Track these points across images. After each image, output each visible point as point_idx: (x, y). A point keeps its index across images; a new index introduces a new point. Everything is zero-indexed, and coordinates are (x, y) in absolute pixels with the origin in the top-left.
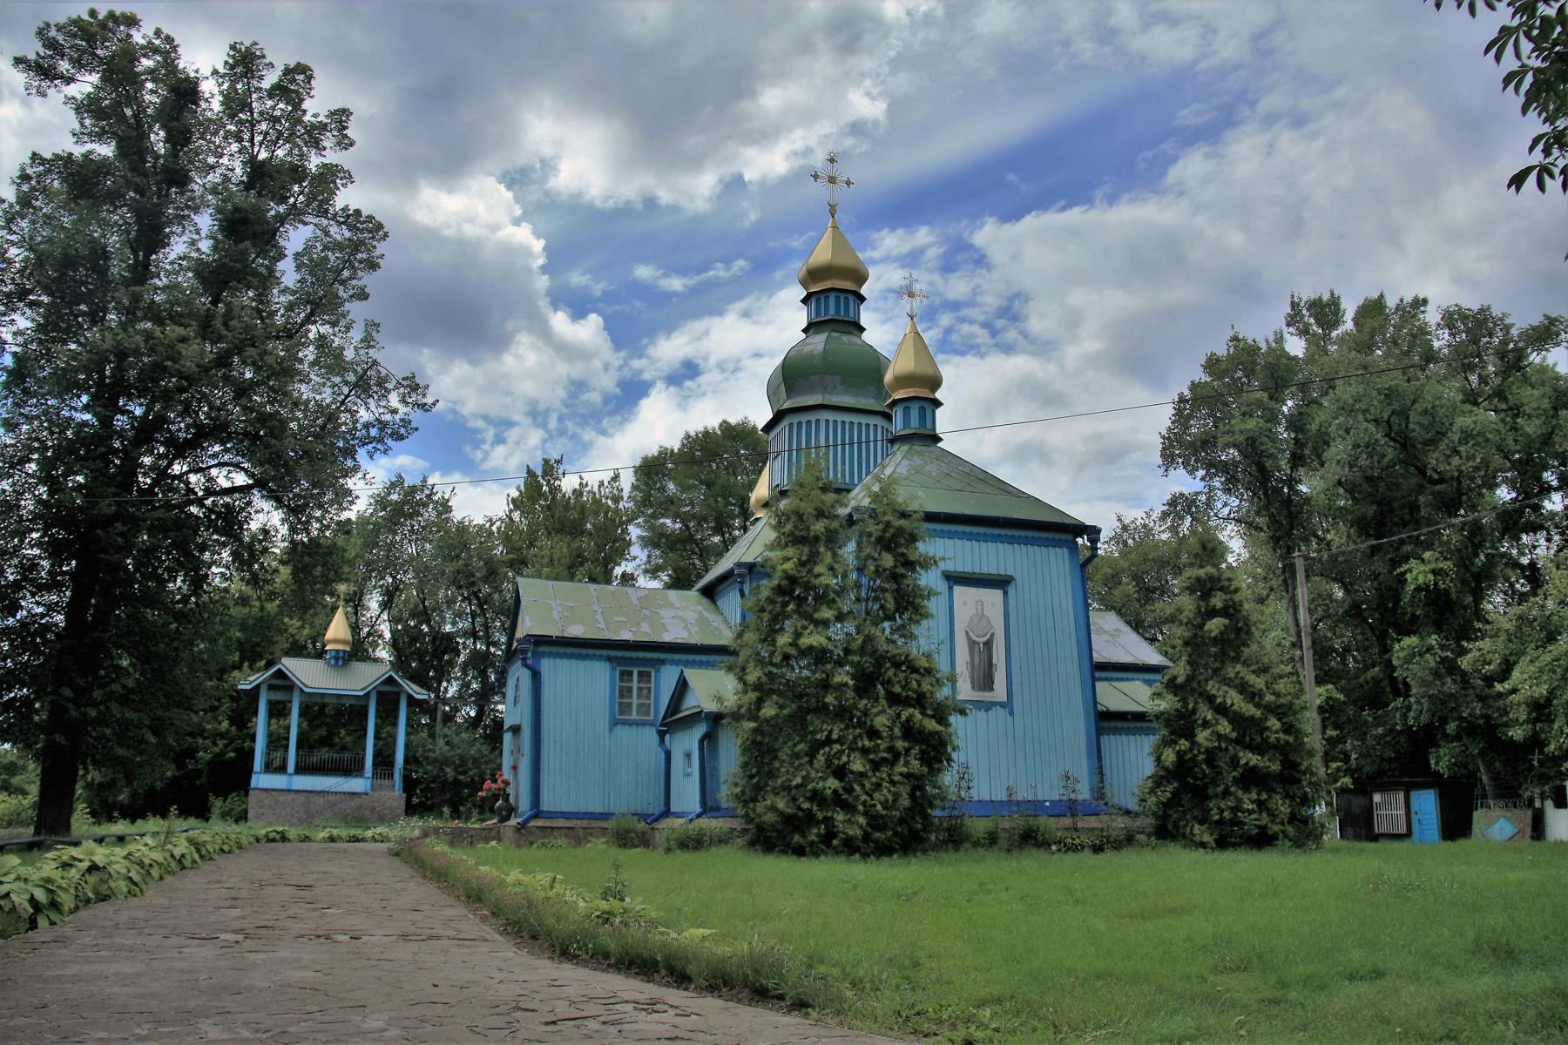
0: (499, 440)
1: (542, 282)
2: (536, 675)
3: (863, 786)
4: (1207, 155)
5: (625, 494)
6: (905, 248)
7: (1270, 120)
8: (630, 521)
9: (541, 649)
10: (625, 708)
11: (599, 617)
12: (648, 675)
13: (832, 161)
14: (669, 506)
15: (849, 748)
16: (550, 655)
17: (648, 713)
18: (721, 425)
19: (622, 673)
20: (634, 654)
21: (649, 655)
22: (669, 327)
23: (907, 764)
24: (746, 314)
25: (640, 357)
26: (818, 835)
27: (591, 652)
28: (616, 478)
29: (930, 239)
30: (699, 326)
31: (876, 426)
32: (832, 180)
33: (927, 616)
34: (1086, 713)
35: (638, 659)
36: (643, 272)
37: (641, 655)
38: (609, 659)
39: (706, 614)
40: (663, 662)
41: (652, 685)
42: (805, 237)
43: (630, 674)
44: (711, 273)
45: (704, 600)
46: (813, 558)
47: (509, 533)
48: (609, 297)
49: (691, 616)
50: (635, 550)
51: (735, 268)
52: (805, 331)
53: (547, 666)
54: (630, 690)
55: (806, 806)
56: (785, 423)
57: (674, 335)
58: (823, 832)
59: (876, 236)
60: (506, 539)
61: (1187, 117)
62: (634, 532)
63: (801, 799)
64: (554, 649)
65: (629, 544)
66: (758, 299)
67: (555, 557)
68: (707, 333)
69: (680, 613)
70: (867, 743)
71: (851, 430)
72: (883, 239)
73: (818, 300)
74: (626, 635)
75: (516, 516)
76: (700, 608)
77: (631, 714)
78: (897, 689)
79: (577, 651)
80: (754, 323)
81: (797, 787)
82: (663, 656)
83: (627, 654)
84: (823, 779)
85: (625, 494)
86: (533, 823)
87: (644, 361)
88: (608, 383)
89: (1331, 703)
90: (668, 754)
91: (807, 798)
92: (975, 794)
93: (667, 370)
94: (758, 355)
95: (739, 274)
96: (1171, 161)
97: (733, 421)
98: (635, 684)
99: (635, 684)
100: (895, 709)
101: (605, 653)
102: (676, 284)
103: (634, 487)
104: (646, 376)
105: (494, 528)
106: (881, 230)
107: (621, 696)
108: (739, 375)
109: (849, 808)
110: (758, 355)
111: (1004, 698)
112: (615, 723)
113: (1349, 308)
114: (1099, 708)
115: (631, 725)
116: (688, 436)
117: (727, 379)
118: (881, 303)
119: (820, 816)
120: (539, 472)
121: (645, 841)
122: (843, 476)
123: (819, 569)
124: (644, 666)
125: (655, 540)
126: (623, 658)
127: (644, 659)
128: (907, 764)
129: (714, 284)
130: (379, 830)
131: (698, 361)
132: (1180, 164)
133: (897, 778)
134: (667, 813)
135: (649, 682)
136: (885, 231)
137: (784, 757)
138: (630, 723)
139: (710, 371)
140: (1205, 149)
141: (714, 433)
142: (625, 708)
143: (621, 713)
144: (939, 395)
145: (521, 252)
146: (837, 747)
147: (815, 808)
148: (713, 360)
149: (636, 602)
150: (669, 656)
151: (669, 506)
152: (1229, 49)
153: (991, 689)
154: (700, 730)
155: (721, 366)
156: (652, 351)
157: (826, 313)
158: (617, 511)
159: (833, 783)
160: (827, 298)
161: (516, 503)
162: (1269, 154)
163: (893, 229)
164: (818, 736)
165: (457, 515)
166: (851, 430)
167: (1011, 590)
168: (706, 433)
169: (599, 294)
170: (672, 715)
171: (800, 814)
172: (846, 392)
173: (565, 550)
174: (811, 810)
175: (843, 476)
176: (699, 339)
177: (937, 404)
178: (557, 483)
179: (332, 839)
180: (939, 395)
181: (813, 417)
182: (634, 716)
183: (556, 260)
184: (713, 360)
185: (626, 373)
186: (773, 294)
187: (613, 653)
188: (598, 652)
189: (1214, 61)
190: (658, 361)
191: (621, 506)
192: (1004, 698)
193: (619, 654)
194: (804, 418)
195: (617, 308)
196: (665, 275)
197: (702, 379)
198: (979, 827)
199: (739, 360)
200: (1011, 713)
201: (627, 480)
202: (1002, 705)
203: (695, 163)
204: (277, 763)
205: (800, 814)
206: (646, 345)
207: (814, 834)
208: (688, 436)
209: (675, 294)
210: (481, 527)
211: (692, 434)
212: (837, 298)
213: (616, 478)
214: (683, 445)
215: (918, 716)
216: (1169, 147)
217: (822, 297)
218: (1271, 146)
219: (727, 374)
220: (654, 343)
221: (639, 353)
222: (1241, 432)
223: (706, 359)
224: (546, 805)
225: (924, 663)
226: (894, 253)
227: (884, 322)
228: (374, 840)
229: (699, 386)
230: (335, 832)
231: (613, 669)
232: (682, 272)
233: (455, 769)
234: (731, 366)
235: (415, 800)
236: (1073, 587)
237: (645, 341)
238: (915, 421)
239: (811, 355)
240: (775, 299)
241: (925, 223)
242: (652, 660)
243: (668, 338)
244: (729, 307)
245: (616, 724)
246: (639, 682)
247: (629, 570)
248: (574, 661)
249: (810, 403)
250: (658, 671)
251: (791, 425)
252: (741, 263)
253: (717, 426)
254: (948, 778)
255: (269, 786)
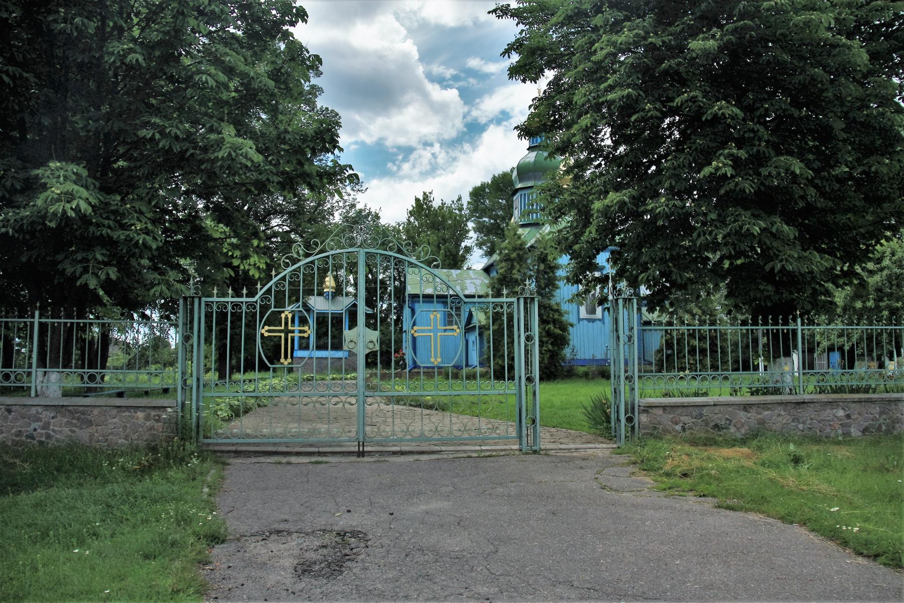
0: (405, 159)
1: (420, 70)
5: (465, 207)
9: (415, 299)
14: (484, 212)
23: (547, 347)
28: (460, 199)
33: (558, 288)
45: (485, 274)
46: (512, 267)
47: (409, 228)
48: (455, 78)
49: (478, 282)
50: (472, 234)
57: (493, 97)
62: (471, 225)
65: (468, 231)
67: (431, 241)
69: (474, 281)
75: (412, 219)
76: (482, 278)
78: (545, 317)
86: (414, 371)
90: (467, 342)
92: (578, 357)
100: (544, 325)
105: (401, 228)
107: (449, 318)
111: (600, 317)
120: (421, 198)
121: (456, 376)
123: (514, 271)
125: (479, 229)
128: (547, 347)
130: (353, 375)
131: (508, 110)
133: (543, 352)
139: (516, 116)
145: (406, 55)
153: (595, 314)
158: (461, 216)
161: (411, 213)
165: (383, 221)
173: (435, 238)
179: (333, 379)
183: (427, 55)
185: (469, 119)
190: (486, 111)
191: (463, 213)
192: (600, 317)
194: (527, 192)
196: (486, 64)
198: (581, 369)
200: (604, 323)
201: (466, 199)
202: (599, 320)
204: (304, 345)
206: (478, 103)
208: (494, 177)
210: (395, 228)
211: (497, 175)
213: (460, 199)
215: (552, 328)
220: (482, 102)
223: (513, 109)
225: (555, 307)
228: (351, 379)
230: (334, 376)
233: (386, 346)
235: (369, 360)
239: (529, 163)
247: (469, 245)
249: (529, 185)
251: (521, 195)
254: (567, 352)
255: (302, 356)
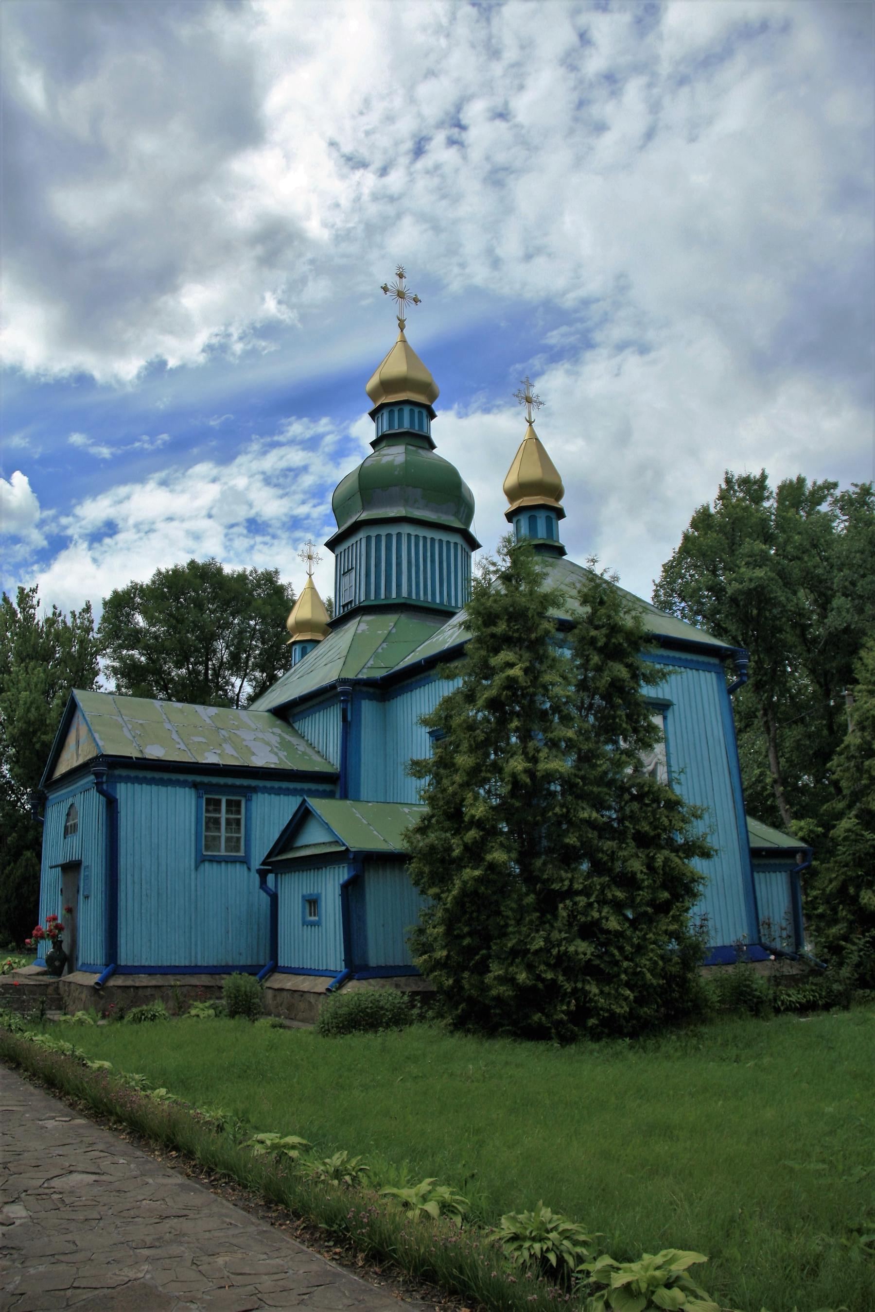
2: (112, 805)
3: (621, 949)
4: (568, 373)
5: (96, 626)
6: (308, 434)
7: (621, 347)
8: (97, 653)
9: (117, 772)
10: (212, 843)
11: (175, 736)
12: (238, 804)
13: (401, 276)
15: (598, 902)
16: (128, 780)
17: (237, 849)
18: (189, 564)
19: (208, 801)
20: (222, 781)
21: (238, 782)
22: (95, 491)
24: (164, 483)
25: (67, 515)
26: (568, 1013)
27: (174, 777)
29: (329, 428)
30: (123, 490)
31: (456, 544)
32: (401, 295)
34: (741, 848)
35: (226, 786)
36: (77, 439)
37: (230, 781)
38: (195, 786)
39: (288, 737)
40: (255, 790)
41: (242, 816)
42: (223, 418)
43: (218, 802)
44: (137, 444)
51: (159, 442)
52: (374, 444)
53: (123, 791)
54: (217, 821)
55: (549, 976)
56: (362, 535)
57: (99, 498)
58: (573, 1007)
59: (284, 421)
60: (720, 526)
61: (554, 338)
63: (542, 967)
64: (133, 773)
65: (96, 674)
66: (176, 471)
68: (128, 497)
70: (620, 894)
71: (433, 546)
72: (290, 424)
73: (391, 413)
74: (211, 758)
76: (278, 731)
77: (219, 851)
78: (645, 827)
79: (157, 775)
80: (172, 491)
81: (537, 952)
82: (253, 783)
83: (215, 780)
84: (570, 941)
85: (96, 626)
87: (70, 519)
88: (38, 539)
89: (812, 835)
90: (274, 899)
91: (548, 965)
93: (90, 529)
94: (170, 519)
95: (161, 447)
96: (539, 374)
97: (200, 561)
98: (223, 816)
99: (223, 816)
101: (191, 778)
102: (105, 452)
103: (105, 619)
104: (69, 532)
106: (289, 417)
108: (152, 536)
109: (603, 977)
110: (170, 519)
112: (201, 860)
113: (773, 484)
114: (752, 845)
115: (219, 862)
116: (159, 573)
117: (141, 539)
118: (281, 480)
119: (568, 987)
122: (418, 594)
124: (234, 794)
126: (211, 785)
127: (233, 786)
129: (140, 454)
132: (545, 377)
134: (275, 968)
135: (238, 812)
136: (293, 418)
137: (510, 913)
138: (217, 860)
139: (128, 531)
140: (567, 366)
141: (183, 572)
142: (212, 843)
143: (207, 848)
144: (562, 503)
146: (582, 900)
147: (561, 978)
148: (131, 522)
149: (208, 721)
150: (260, 783)
151: (135, 638)
152: (594, 285)
154: (341, 874)
155: (137, 526)
156: (78, 511)
157: (401, 424)
159: (583, 948)
160: (401, 411)
162: (617, 375)
163: (300, 417)
164: (556, 886)
166: (433, 546)
167: (670, 715)
168: (176, 571)
169: (37, 456)
170: (283, 850)
171: (540, 985)
172: (426, 507)
174: (554, 981)
175: (418, 594)
176: (120, 502)
177: (560, 514)
178: (32, 611)
180: (562, 503)
181: (393, 530)
182: (223, 853)
184: (131, 522)
186: (190, 467)
187: (199, 779)
188: (182, 777)
189: (582, 293)
193: (206, 779)
194: (383, 531)
195: (50, 470)
196: (95, 444)
197: (120, 537)
199: (153, 523)
201: (98, 613)
203: (122, 349)
205: (540, 985)
207: (561, 1011)
208: (159, 573)
209: (104, 460)
211: (163, 570)
212: (412, 412)
213: (88, 609)
214: (154, 582)
216: (536, 362)
217: (396, 409)
218: (619, 368)
219: (142, 534)
220: (80, 503)
221: (67, 511)
222: (751, 580)
223: (125, 520)
224: (125, 958)
226: (299, 438)
227: (281, 497)
229: (116, 544)
231: (199, 797)
232: (109, 443)
234: (146, 527)
236: (721, 714)
237: (74, 501)
238: (542, 532)
240: (191, 471)
241: (325, 415)
242: (241, 787)
243: (94, 500)
244: (151, 476)
245: (203, 861)
246: (228, 812)
248: (155, 788)
250: (249, 800)
252: (165, 437)
253: (186, 565)
